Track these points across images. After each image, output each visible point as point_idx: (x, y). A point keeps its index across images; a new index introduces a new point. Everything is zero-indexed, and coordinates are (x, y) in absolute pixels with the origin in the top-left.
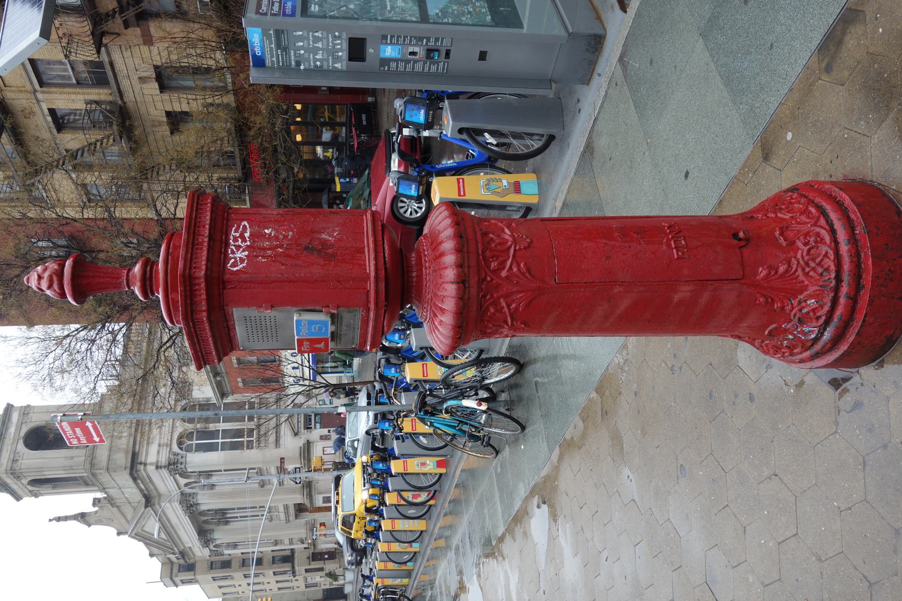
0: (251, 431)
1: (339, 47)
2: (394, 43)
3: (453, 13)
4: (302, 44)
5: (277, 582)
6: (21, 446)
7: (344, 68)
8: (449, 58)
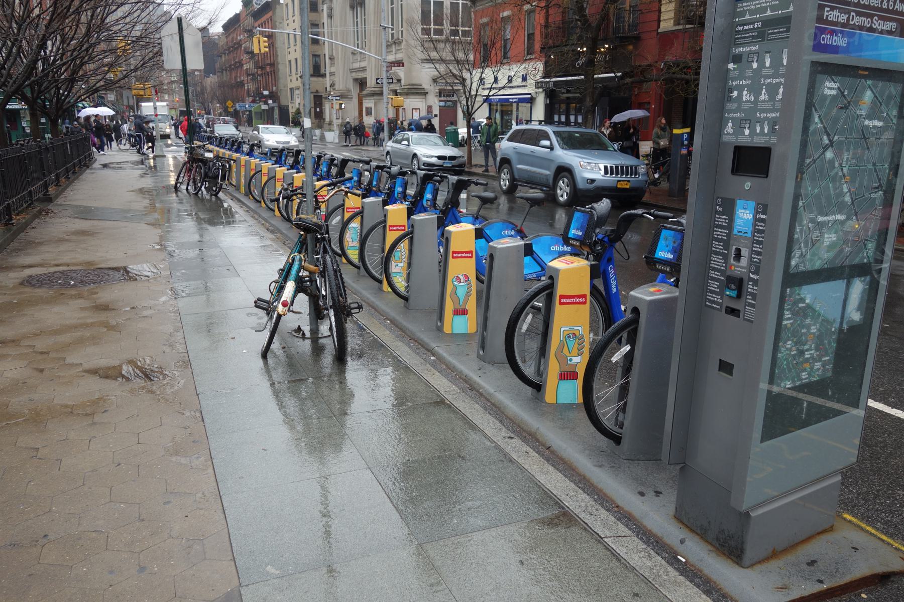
0: (439, 32)
1: (758, 131)
4: (768, 64)
5: (296, 60)
7: (725, 139)
8: (727, 312)
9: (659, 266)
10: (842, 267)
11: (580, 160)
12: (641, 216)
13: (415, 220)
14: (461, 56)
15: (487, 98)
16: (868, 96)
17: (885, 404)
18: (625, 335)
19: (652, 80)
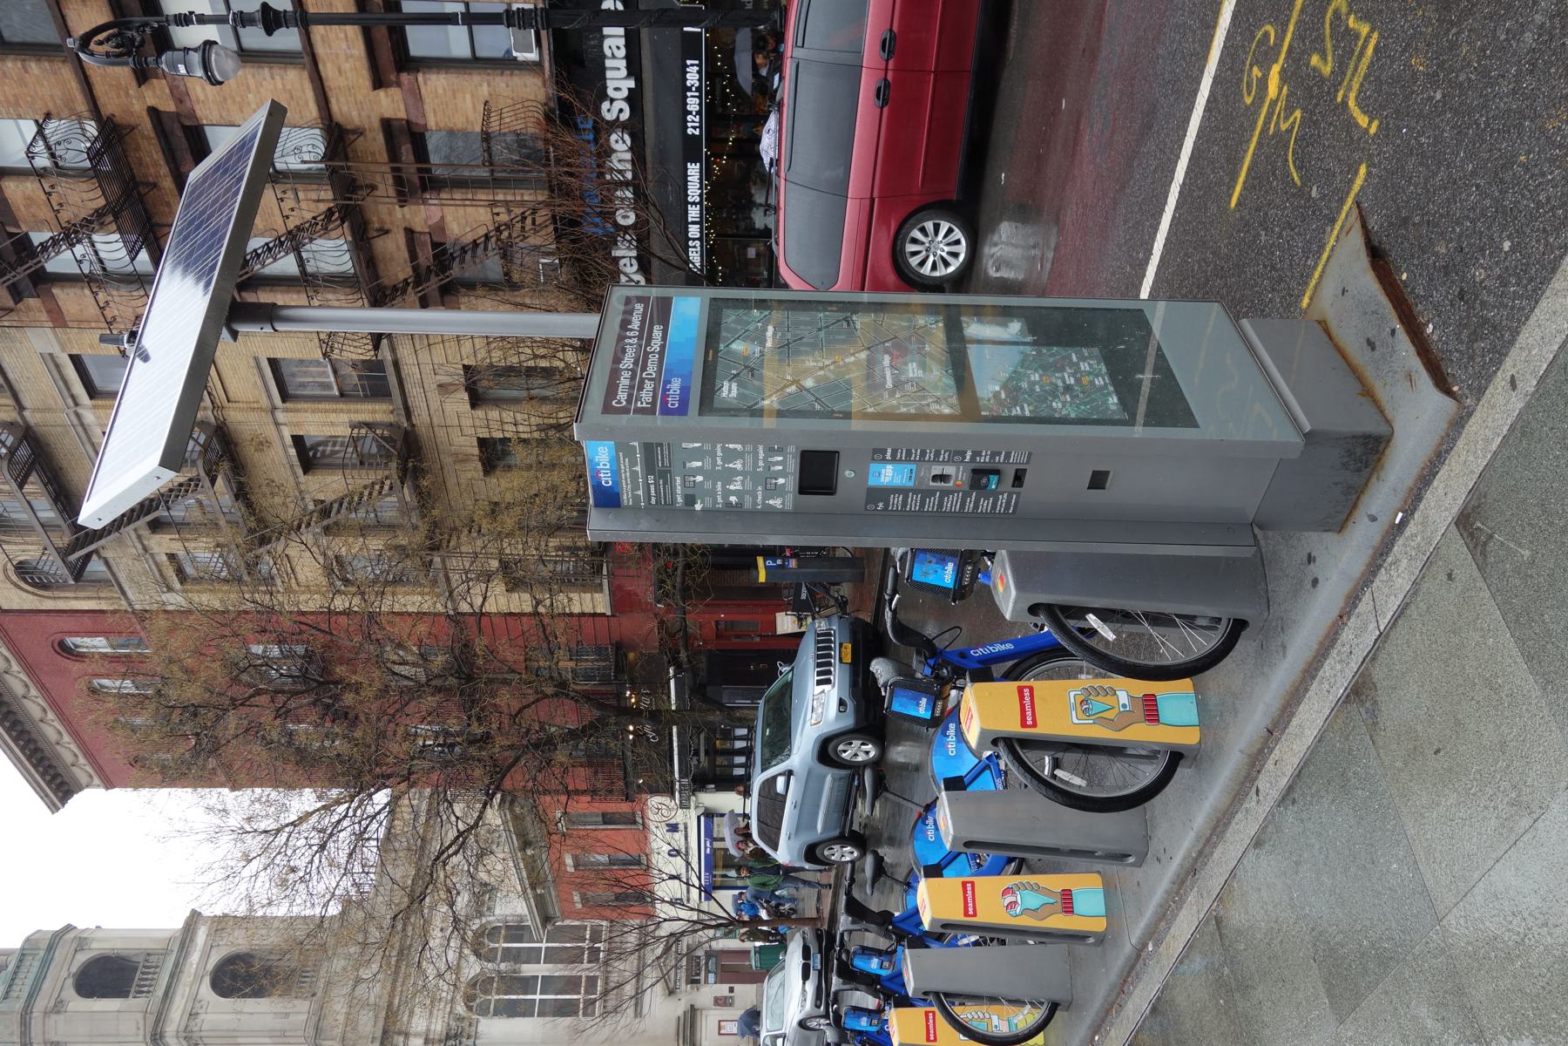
0: (592, 981)
2: (901, 460)
3: (1031, 392)
4: (699, 464)
6: (206, 989)
9: (966, 582)
10: (951, 352)
11: (808, 724)
12: (894, 612)
13: (915, 990)
14: (632, 939)
15: (706, 891)
16: (738, 346)
17: (1147, 263)
18: (1072, 624)
19: (684, 619)
